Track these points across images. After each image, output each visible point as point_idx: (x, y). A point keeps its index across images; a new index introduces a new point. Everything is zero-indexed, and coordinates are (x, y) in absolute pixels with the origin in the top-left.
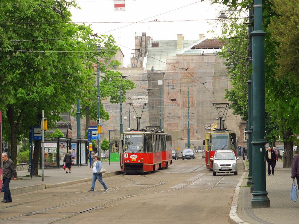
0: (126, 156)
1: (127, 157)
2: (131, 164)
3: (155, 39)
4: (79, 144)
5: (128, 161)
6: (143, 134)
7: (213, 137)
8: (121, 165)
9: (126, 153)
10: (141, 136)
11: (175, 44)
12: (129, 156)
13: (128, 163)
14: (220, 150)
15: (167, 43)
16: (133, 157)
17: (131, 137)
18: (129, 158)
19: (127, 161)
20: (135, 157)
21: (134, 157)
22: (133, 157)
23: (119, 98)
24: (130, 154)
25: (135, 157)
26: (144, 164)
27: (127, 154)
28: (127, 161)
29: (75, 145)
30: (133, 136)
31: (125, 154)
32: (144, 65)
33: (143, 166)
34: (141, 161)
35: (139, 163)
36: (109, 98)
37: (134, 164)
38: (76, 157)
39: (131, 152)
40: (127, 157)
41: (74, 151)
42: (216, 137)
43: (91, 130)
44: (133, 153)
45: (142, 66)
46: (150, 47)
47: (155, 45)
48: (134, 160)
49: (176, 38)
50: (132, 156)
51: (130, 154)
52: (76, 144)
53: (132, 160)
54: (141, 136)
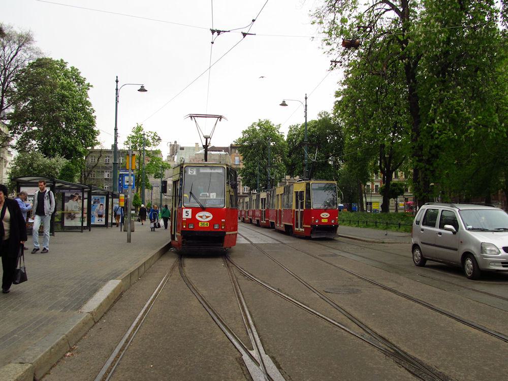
0: (187, 214)
1: (190, 217)
2: (198, 232)
3: (182, 146)
4: (110, 200)
5: (192, 227)
6: (225, 167)
7: (313, 188)
8: (173, 233)
9: (186, 208)
10: (221, 171)
11: (194, 149)
12: (194, 214)
13: (191, 232)
14: (443, 202)
15: (189, 148)
16: (201, 217)
17: (198, 171)
18: (193, 220)
19: (187, 225)
20: (207, 217)
21: (205, 218)
22: (201, 217)
23: (161, 174)
24: (195, 211)
25: (207, 217)
26: (227, 233)
27: (190, 211)
28: (187, 225)
29: (103, 198)
30: (202, 170)
31: (184, 211)
32: (175, 160)
33: (226, 238)
34: (220, 226)
35: (216, 232)
36: (153, 175)
37: (204, 232)
38: (104, 215)
39: (197, 205)
40: (190, 217)
41: (102, 206)
42: (317, 188)
43: (123, 174)
44: (203, 209)
45: (174, 160)
46: (179, 150)
47: (182, 149)
48: (206, 223)
49: (194, 145)
50: (201, 214)
51: (195, 211)
52: (105, 197)
53: (200, 224)
54: (221, 171)
